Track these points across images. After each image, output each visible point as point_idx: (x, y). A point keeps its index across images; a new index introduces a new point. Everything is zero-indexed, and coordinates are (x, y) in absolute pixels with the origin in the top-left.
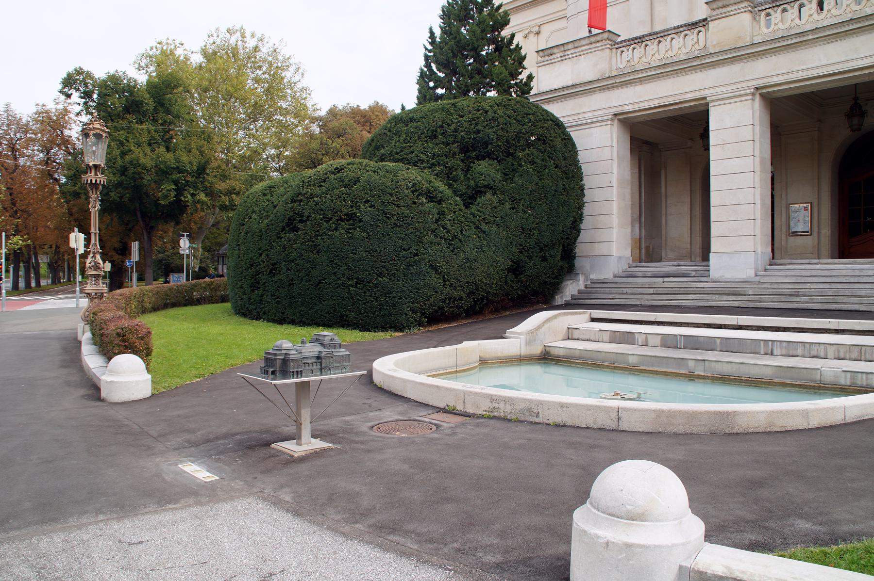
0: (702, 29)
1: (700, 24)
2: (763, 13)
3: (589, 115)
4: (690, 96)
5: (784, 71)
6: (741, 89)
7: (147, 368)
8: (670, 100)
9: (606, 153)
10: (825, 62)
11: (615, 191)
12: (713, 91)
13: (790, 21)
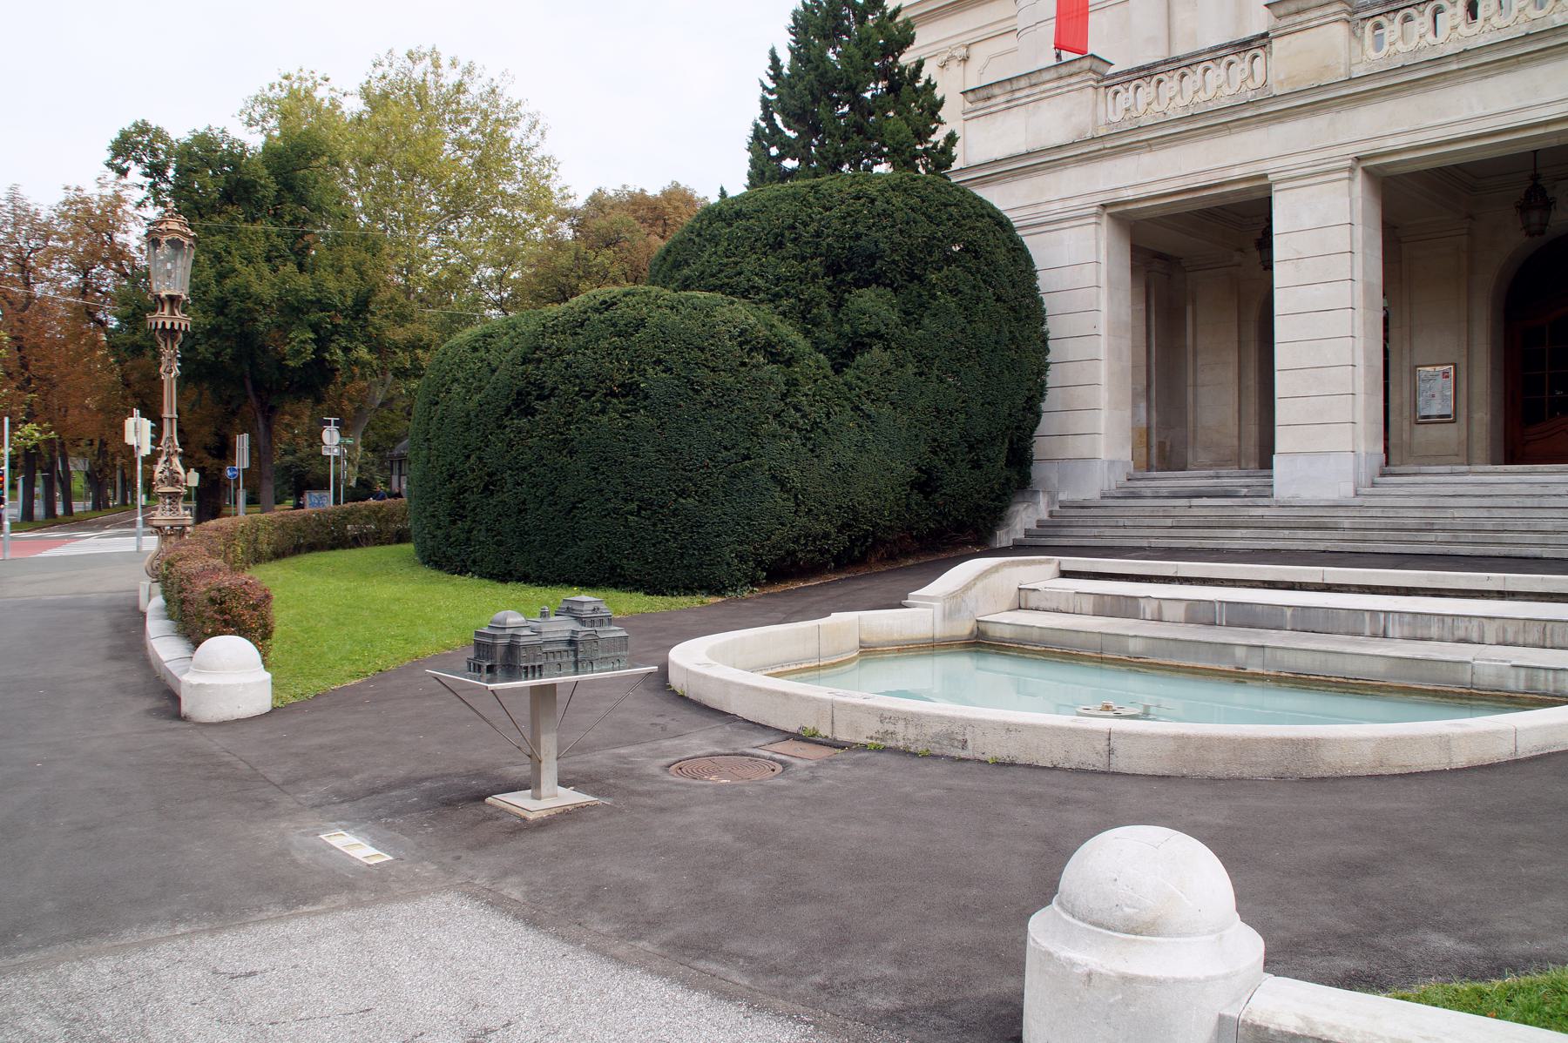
0: (1259, 52)
1: (1256, 44)
2: (1369, 24)
3: (1057, 206)
4: (1237, 173)
5: (1406, 128)
6: (1330, 160)
7: (264, 661)
8: (1202, 180)
9: (1088, 275)
10: (1479, 111)
11: (1103, 342)
12: (1279, 163)
13: (1417, 38)
